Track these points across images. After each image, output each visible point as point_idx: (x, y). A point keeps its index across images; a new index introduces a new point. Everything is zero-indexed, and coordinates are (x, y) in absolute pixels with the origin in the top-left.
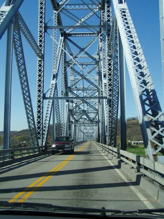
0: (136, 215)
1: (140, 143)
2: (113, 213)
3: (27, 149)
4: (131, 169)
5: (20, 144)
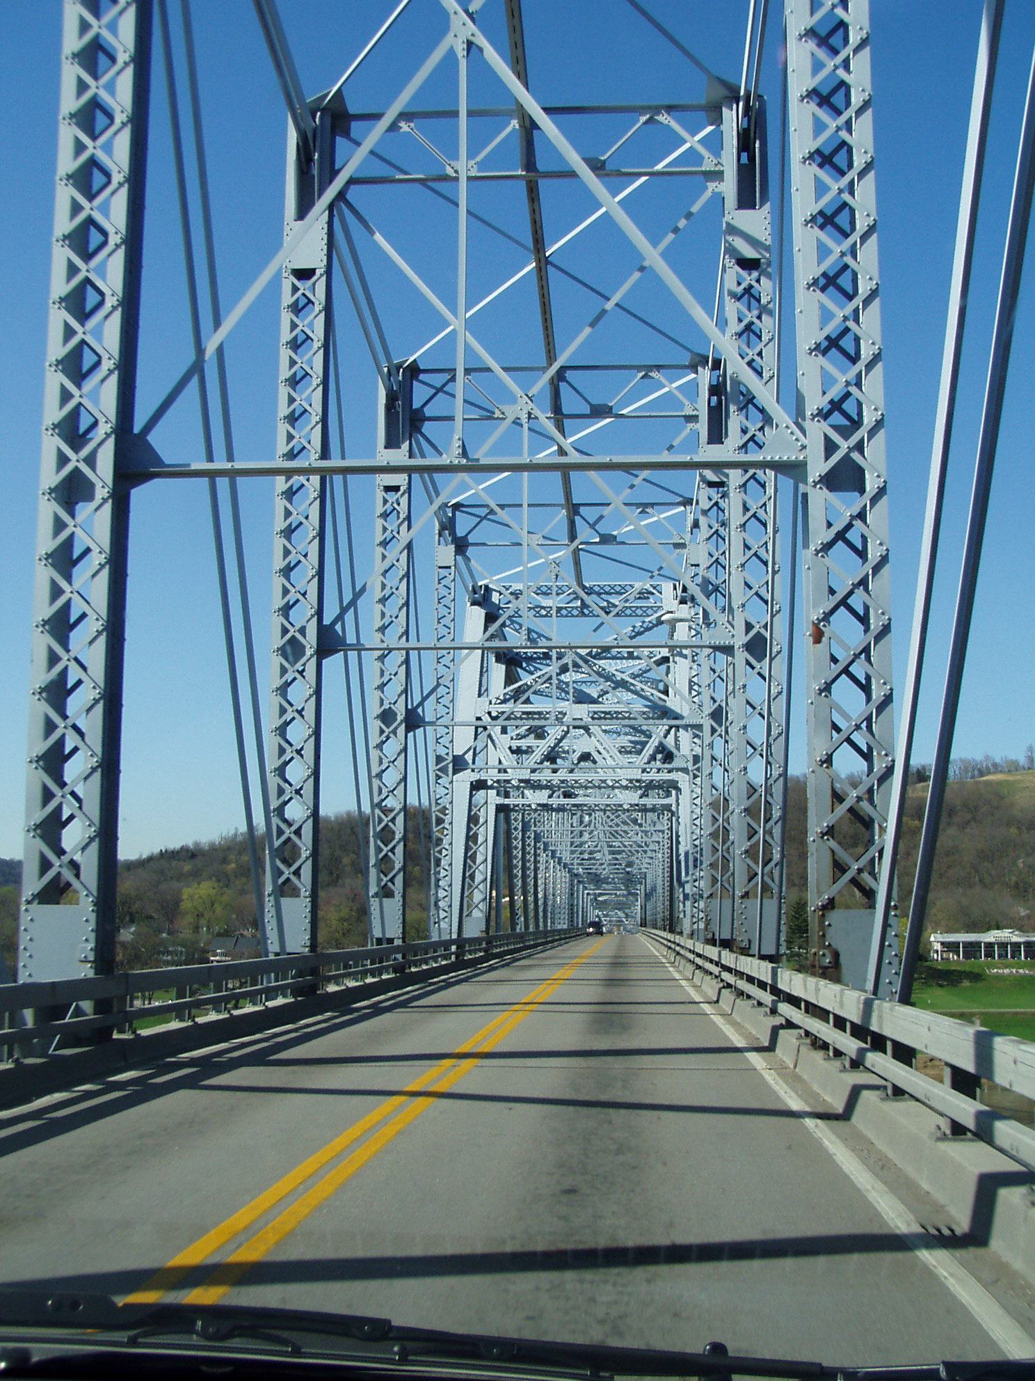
1: (990, 946)
4: (944, 1138)
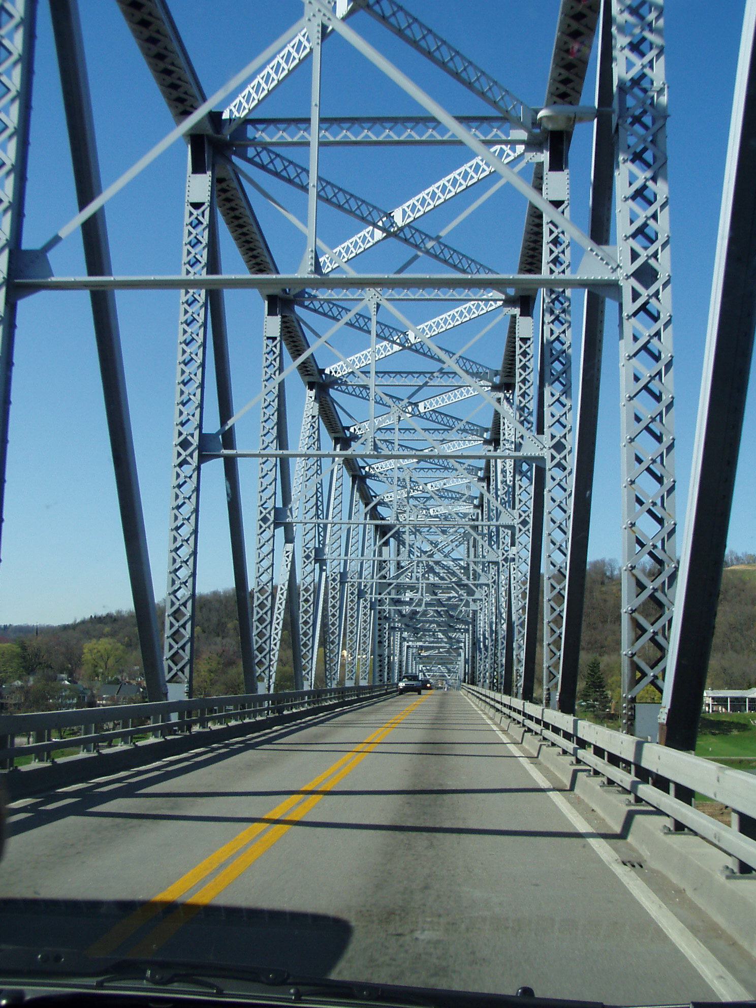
4: (731, 875)
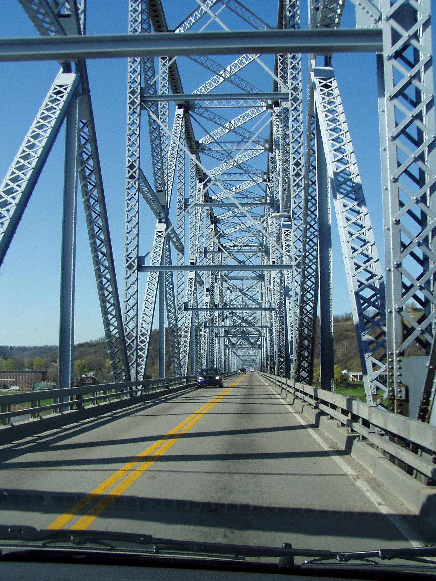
0: (376, 563)
2: (312, 558)
3: (106, 389)
4: (339, 426)
5: (82, 379)
